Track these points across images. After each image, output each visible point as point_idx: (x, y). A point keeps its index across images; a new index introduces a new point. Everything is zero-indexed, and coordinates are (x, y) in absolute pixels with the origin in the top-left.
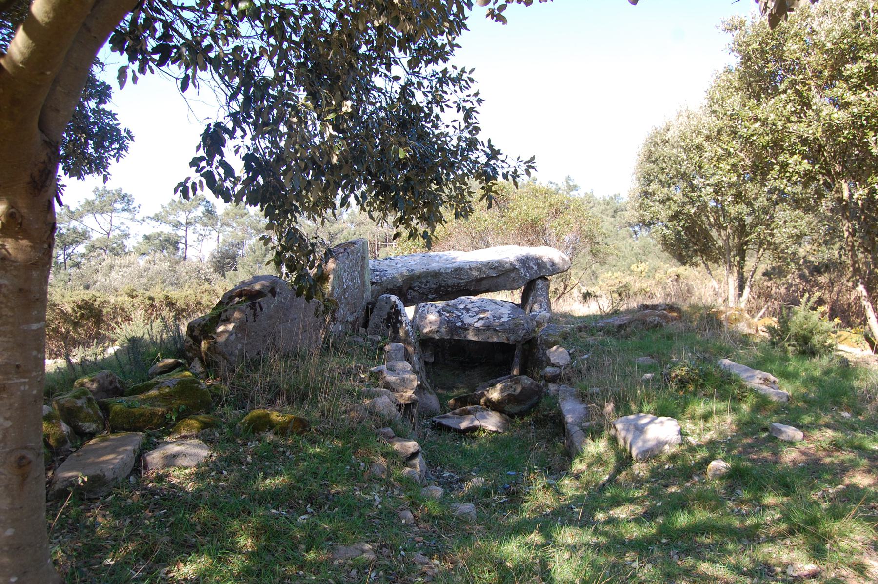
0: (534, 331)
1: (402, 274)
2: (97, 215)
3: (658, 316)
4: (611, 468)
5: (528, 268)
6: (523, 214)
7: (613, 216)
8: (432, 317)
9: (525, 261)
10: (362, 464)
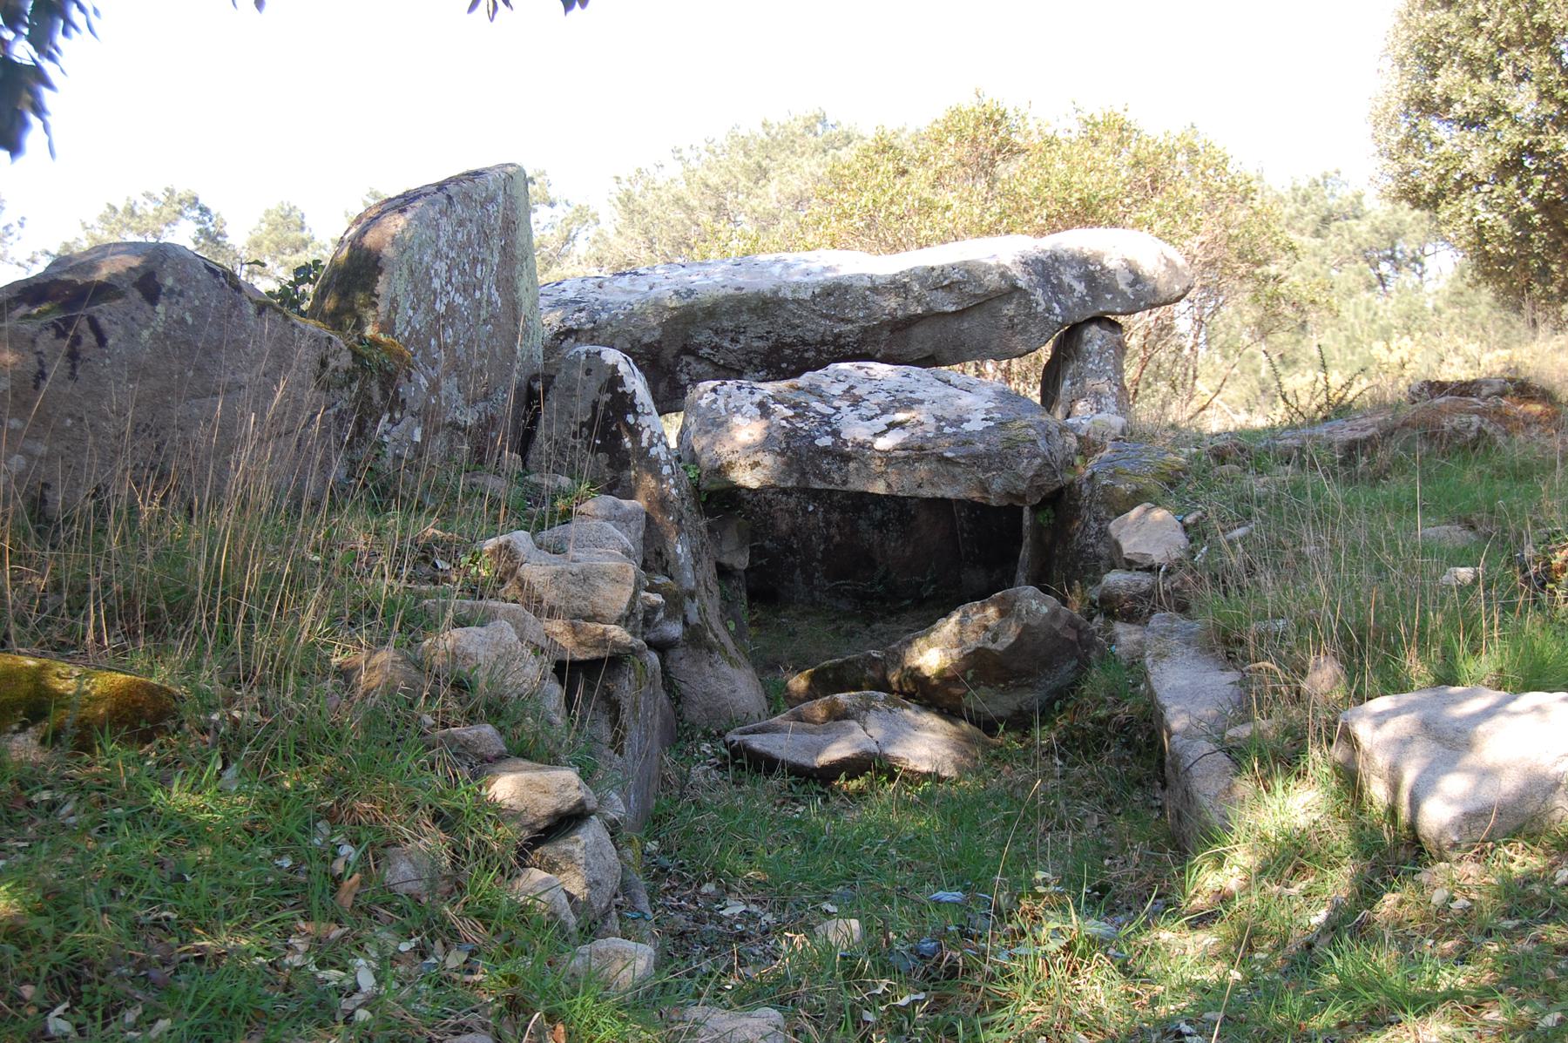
0: (1069, 465)
1: (657, 303)
3: (1482, 413)
4: (1339, 882)
5: (1057, 290)
6: (1054, 184)
7: (1317, 234)
8: (740, 432)
9: (1046, 269)
10: (347, 849)
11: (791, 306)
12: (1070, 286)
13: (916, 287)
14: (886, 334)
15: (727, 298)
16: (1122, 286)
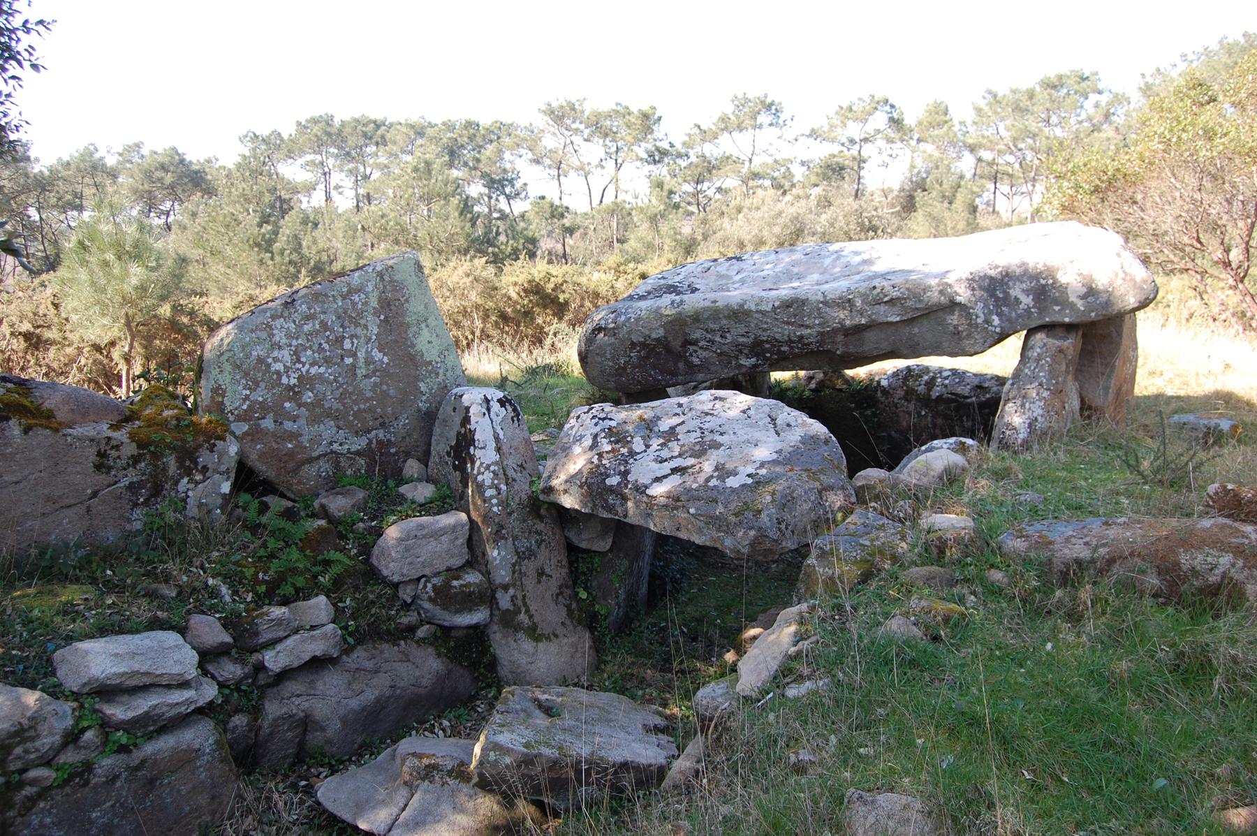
2: (735, 134)
11: (756, 315)
12: (1016, 299)
13: (859, 303)
14: (840, 338)
15: (705, 309)
16: (1073, 298)
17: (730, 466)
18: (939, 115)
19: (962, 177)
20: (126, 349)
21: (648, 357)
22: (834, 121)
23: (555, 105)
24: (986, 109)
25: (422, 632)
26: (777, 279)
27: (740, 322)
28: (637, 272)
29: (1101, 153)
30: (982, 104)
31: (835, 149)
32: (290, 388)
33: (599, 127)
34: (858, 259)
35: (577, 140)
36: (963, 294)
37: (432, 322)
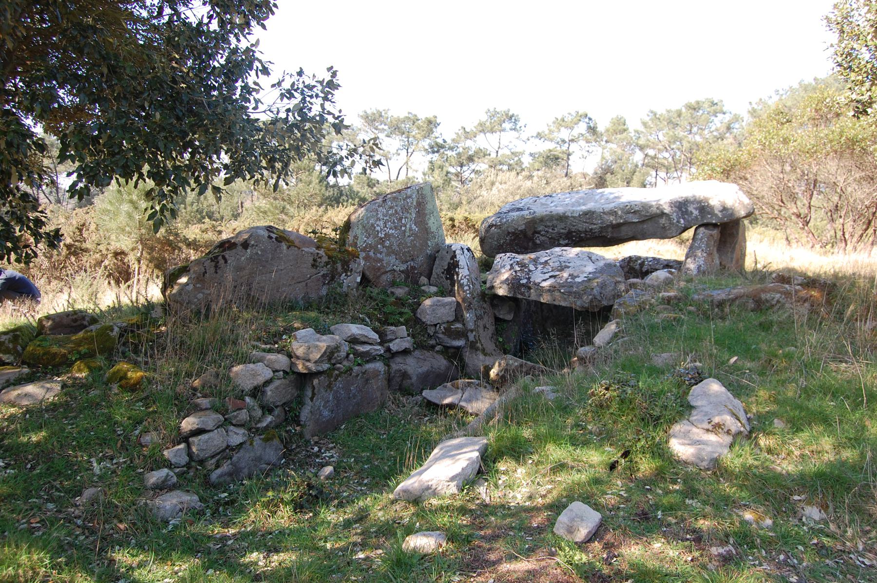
2: (488, 134)
13: (620, 213)
14: (610, 229)
15: (546, 215)
16: (716, 212)
17: (575, 274)
18: (619, 127)
19: (637, 166)
20: (139, 255)
21: (514, 240)
22: (552, 128)
23: (369, 112)
24: (650, 123)
25: (438, 348)
26: (573, 205)
27: (562, 222)
28: (447, 217)
29: (727, 148)
30: (647, 119)
31: (550, 146)
32: (381, 239)
33: (397, 128)
34: (612, 196)
35: (382, 136)
36: (667, 210)
37: (435, 214)
